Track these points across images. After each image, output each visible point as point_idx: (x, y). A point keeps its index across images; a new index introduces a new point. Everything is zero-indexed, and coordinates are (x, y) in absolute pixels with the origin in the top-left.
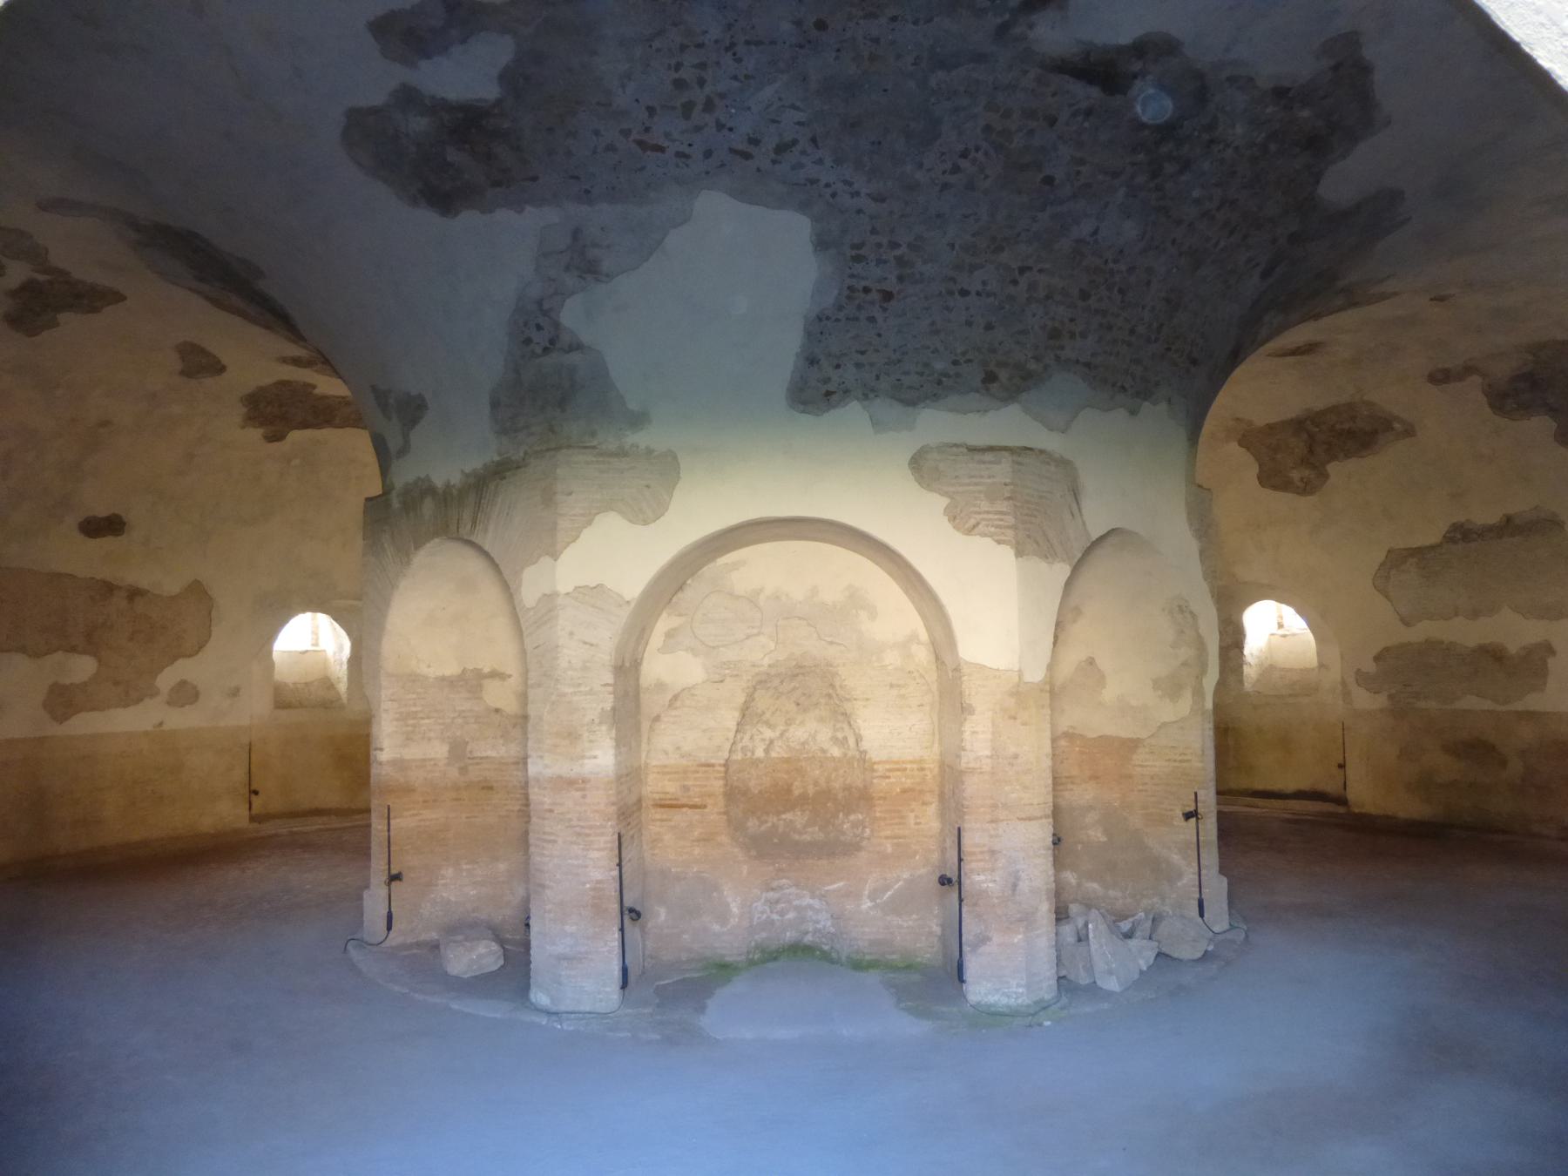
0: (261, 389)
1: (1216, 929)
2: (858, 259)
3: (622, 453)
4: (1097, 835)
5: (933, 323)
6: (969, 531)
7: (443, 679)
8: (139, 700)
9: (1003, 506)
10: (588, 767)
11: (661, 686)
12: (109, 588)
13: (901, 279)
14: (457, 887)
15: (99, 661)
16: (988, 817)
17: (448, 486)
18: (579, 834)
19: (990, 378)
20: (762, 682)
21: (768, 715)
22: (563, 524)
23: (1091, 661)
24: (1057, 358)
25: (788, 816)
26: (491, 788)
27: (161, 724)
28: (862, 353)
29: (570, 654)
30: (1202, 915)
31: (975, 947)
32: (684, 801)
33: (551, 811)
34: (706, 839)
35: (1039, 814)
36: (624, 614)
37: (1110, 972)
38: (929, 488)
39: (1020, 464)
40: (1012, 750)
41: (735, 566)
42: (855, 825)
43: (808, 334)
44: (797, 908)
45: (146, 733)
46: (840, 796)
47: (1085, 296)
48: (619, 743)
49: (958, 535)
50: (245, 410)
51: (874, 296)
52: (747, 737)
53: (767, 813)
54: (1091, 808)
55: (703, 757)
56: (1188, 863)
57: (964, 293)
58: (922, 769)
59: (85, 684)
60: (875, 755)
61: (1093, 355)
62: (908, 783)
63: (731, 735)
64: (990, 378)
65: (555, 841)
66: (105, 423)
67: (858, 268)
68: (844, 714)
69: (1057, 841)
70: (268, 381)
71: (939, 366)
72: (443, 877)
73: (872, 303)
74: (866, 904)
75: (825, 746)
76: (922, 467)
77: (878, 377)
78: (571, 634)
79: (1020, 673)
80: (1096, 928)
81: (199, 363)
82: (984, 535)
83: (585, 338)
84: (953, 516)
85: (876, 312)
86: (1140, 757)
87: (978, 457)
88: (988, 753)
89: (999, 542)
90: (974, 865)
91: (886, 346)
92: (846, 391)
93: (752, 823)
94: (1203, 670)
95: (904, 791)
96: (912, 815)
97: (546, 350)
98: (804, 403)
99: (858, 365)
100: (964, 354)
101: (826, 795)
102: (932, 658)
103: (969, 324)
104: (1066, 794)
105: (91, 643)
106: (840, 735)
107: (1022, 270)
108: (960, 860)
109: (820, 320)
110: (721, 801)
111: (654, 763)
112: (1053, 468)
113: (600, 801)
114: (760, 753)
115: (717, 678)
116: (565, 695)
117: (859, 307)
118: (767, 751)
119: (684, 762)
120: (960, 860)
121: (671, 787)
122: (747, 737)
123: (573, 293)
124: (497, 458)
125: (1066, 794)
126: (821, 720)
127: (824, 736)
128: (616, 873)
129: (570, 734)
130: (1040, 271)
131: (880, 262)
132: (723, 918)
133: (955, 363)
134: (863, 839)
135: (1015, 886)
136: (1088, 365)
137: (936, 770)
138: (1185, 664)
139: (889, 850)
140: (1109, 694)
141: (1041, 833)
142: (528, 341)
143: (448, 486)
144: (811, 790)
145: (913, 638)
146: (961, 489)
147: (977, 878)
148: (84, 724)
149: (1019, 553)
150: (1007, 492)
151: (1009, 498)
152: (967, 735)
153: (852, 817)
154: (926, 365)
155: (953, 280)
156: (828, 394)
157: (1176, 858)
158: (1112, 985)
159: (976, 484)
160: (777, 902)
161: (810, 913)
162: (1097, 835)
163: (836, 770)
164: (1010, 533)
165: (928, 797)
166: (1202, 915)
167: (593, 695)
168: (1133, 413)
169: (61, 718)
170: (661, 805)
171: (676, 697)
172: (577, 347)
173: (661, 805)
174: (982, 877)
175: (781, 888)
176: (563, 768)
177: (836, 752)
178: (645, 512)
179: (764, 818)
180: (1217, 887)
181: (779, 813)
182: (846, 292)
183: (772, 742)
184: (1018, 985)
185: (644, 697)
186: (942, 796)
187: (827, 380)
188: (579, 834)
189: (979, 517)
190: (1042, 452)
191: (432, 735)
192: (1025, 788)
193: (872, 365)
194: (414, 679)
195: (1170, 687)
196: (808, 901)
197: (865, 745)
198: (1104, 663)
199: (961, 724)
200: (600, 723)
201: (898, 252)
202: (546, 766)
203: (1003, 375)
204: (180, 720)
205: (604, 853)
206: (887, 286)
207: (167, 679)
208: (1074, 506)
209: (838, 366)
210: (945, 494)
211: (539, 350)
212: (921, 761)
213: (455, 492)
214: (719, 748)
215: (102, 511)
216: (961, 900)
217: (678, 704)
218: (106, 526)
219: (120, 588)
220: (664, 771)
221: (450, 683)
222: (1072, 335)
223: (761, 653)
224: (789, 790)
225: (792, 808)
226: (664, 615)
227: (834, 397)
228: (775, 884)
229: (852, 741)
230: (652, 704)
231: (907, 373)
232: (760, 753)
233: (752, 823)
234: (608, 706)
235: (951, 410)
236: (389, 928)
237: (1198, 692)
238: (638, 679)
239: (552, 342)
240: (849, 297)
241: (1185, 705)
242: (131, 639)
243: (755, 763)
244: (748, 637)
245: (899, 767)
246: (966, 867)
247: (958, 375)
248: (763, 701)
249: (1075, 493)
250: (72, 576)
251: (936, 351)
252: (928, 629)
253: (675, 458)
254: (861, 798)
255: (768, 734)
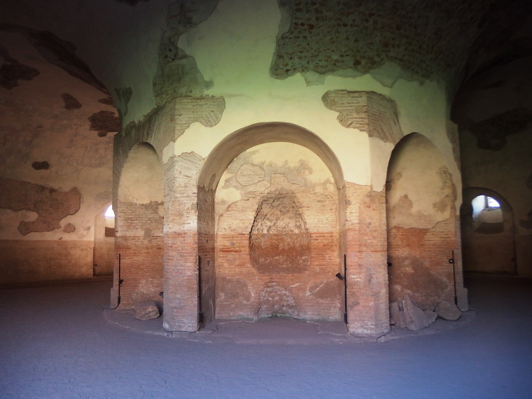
0: (95, 114)
1: (463, 310)
2: (298, 10)
3: (202, 98)
4: (409, 270)
5: (331, 39)
6: (348, 126)
7: (143, 205)
8: (53, 229)
9: (363, 115)
10: (186, 227)
11: (223, 202)
12: (43, 188)
13: (317, 19)
14: (146, 287)
15: (39, 214)
16: (358, 250)
17: (140, 122)
18: (182, 256)
19: (357, 63)
20: (264, 201)
21: (268, 216)
22: (178, 127)
23: (406, 197)
24: (387, 56)
25: (277, 258)
26: (160, 248)
27: (61, 238)
28: (302, 52)
29: (180, 181)
30: (456, 304)
31: (352, 308)
32: (233, 249)
33: (171, 247)
34: (241, 265)
35: (380, 249)
36: (201, 165)
37: (412, 322)
38: (330, 108)
39: (370, 97)
40: (368, 221)
41: (254, 153)
42: (304, 261)
43: (278, 45)
44: (279, 295)
45: (55, 241)
46: (299, 249)
47: (399, 28)
48: (200, 219)
49: (344, 129)
50: (90, 123)
51: (306, 27)
52: (259, 224)
53: (268, 256)
54: (407, 258)
55: (240, 231)
56: (448, 273)
57: (345, 25)
58: (332, 236)
59: (33, 223)
60: (312, 230)
61: (403, 56)
62: (326, 242)
63: (252, 222)
64: (357, 63)
65: (173, 259)
66: (41, 127)
67: (299, 14)
68: (300, 214)
69: (389, 264)
70: (97, 111)
71: (335, 57)
72: (141, 283)
73: (305, 30)
74: (308, 293)
75: (292, 229)
76: (327, 99)
77: (308, 63)
78: (180, 172)
79: (371, 186)
80: (406, 302)
81: (71, 103)
82: (355, 128)
83: (188, 52)
84: (341, 120)
85: (307, 34)
86: (428, 236)
87: (352, 95)
88: (357, 222)
89: (361, 131)
90: (351, 271)
91: (312, 49)
92: (295, 69)
93: (262, 260)
94: (455, 198)
95: (324, 246)
96: (328, 256)
97: (173, 60)
98: (277, 75)
99: (300, 58)
100: (346, 52)
101: (292, 249)
102: (336, 189)
103: (347, 39)
104: (396, 252)
105: (36, 209)
106: (298, 224)
107: (371, 15)
108: (346, 269)
109: (283, 38)
110: (247, 249)
111: (220, 233)
112: (385, 102)
113: (191, 242)
114: (265, 232)
115: (246, 198)
116: (176, 198)
117: (300, 32)
118: (268, 231)
119: (232, 233)
120: (346, 269)
121: (227, 244)
122: (259, 224)
123: (182, 33)
124: (156, 107)
125: (396, 252)
126: (290, 218)
127: (292, 225)
128: (197, 273)
129: (179, 214)
130: (379, 16)
131: (308, 11)
132: (248, 298)
133: (342, 56)
134: (307, 266)
135: (370, 280)
136: (401, 60)
137: (338, 237)
138: (447, 196)
139: (318, 271)
140: (415, 209)
141: (381, 259)
142: (166, 57)
143: (140, 122)
144: (286, 248)
145: (328, 181)
146: (344, 108)
147: (353, 277)
148: (35, 236)
149: (370, 136)
150: (365, 109)
151: (365, 112)
152: (348, 214)
153: (303, 258)
154: (329, 57)
155: (340, 19)
156: (287, 71)
157: (445, 279)
158: (413, 327)
159: (351, 106)
160: (271, 292)
161: (285, 297)
162: (409, 270)
163: (297, 239)
164: (366, 126)
165: (334, 248)
166: (456, 304)
167: (189, 198)
168: (422, 84)
169: (25, 234)
170: (223, 251)
171: (229, 206)
172: (185, 56)
173: (223, 251)
174: (355, 276)
175: (272, 286)
176: (176, 228)
177: (297, 231)
178: (210, 123)
179: (267, 258)
180: (463, 292)
181: (273, 257)
182: (294, 25)
183: (270, 227)
184: (372, 325)
185: (216, 207)
186: (340, 248)
187: (287, 65)
188: (182, 256)
189: (352, 120)
190: (380, 95)
191: (138, 227)
192: (374, 238)
193: (306, 57)
194: (131, 204)
195: (441, 207)
196: (284, 292)
197: (308, 226)
198: (412, 197)
199: (346, 209)
200: (192, 209)
201: (315, 7)
202: (170, 228)
203: (363, 62)
204: (68, 237)
205: (191, 264)
206: (311, 22)
207: (63, 223)
208: (395, 119)
209: (291, 58)
210: (338, 111)
211: (170, 60)
212: (332, 233)
213: (142, 124)
214: (247, 227)
215: (40, 160)
216: (346, 287)
217: (230, 209)
218: (45, 165)
219: (47, 188)
220: (224, 237)
221: (146, 207)
222: (393, 46)
223: (263, 188)
224: (277, 247)
225: (279, 255)
226: (225, 173)
227: (290, 72)
228: (270, 284)
229: (303, 226)
230: (219, 209)
231: (321, 61)
232: (265, 232)
233: (262, 260)
234: (195, 202)
235: (340, 76)
236: (119, 303)
237: (453, 208)
238: (214, 199)
239: (175, 56)
240: (295, 28)
241: (447, 214)
242: (50, 207)
243: (263, 235)
244: (259, 182)
245: (322, 235)
246: (348, 272)
247: (343, 61)
248: (266, 209)
249: (396, 114)
250: (30, 183)
251: (333, 51)
252: (334, 176)
253: (224, 99)
254: (306, 249)
255: (269, 224)
